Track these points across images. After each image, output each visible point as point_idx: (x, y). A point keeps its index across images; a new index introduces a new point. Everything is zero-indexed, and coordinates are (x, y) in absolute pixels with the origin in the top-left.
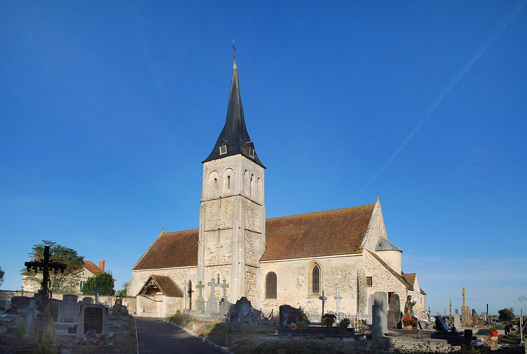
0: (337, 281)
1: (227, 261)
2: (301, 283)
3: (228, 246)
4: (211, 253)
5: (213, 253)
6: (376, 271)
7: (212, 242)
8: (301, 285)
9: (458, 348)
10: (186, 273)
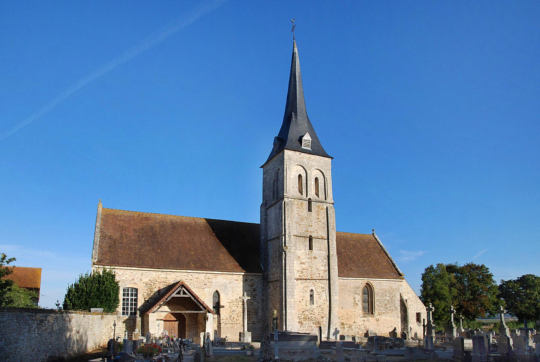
0: (386, 302)
1: (321, 275)
2: (357, 302)
3: (323, 259)
4: (302, 263)
5: (303, 263)
6: (409, 295)
7: (303, 251)
8: (357, 304)
9: (257, 345)
10: (210, 280)
